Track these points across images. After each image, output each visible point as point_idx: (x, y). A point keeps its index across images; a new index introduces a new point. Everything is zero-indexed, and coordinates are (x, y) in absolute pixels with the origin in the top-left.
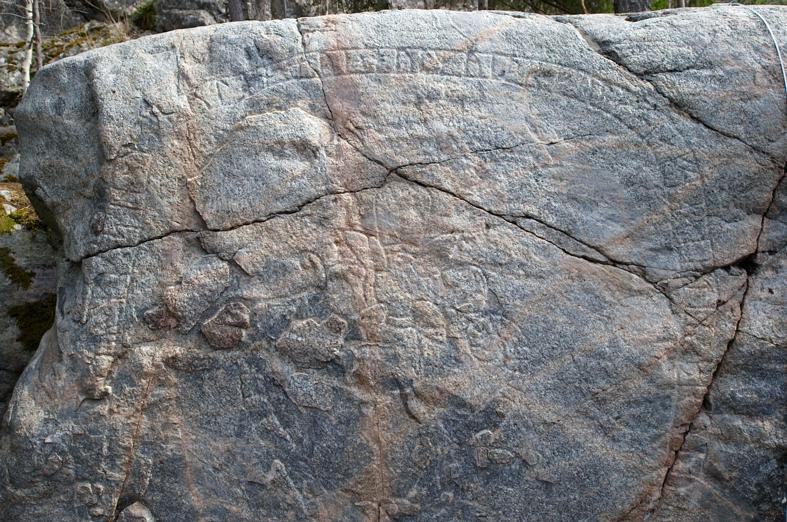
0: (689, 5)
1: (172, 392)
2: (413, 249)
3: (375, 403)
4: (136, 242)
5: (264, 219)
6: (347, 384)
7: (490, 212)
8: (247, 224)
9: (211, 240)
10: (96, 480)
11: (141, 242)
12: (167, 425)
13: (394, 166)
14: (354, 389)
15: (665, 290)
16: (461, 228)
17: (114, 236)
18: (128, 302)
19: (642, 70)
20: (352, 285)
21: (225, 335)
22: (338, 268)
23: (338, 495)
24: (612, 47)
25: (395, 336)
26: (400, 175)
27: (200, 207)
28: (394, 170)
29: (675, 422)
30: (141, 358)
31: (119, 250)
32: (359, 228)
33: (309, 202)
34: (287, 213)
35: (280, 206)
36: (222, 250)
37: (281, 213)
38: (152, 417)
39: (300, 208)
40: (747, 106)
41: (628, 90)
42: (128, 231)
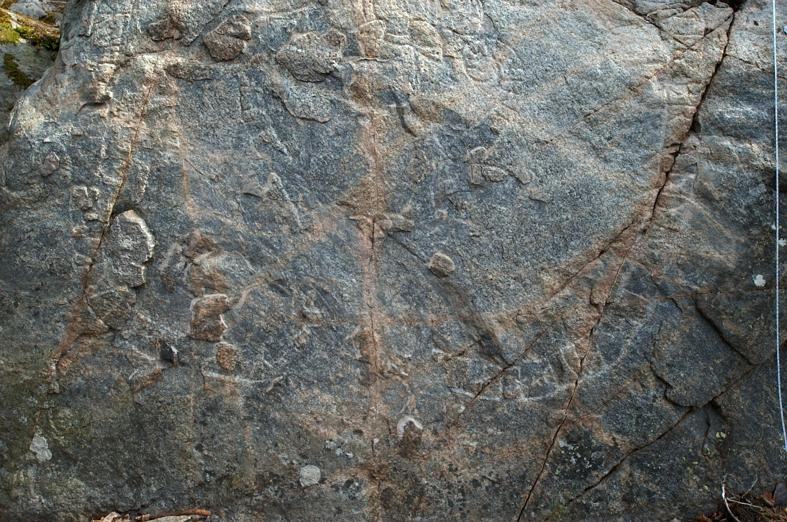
1: (172, 100)
3: (372, 115)
6: (344, 96)
12: (165, 133)
14: (351, 103)
18: (132, 17)
21: (227, 45)
29: (665, 142)
38: (151, 124)
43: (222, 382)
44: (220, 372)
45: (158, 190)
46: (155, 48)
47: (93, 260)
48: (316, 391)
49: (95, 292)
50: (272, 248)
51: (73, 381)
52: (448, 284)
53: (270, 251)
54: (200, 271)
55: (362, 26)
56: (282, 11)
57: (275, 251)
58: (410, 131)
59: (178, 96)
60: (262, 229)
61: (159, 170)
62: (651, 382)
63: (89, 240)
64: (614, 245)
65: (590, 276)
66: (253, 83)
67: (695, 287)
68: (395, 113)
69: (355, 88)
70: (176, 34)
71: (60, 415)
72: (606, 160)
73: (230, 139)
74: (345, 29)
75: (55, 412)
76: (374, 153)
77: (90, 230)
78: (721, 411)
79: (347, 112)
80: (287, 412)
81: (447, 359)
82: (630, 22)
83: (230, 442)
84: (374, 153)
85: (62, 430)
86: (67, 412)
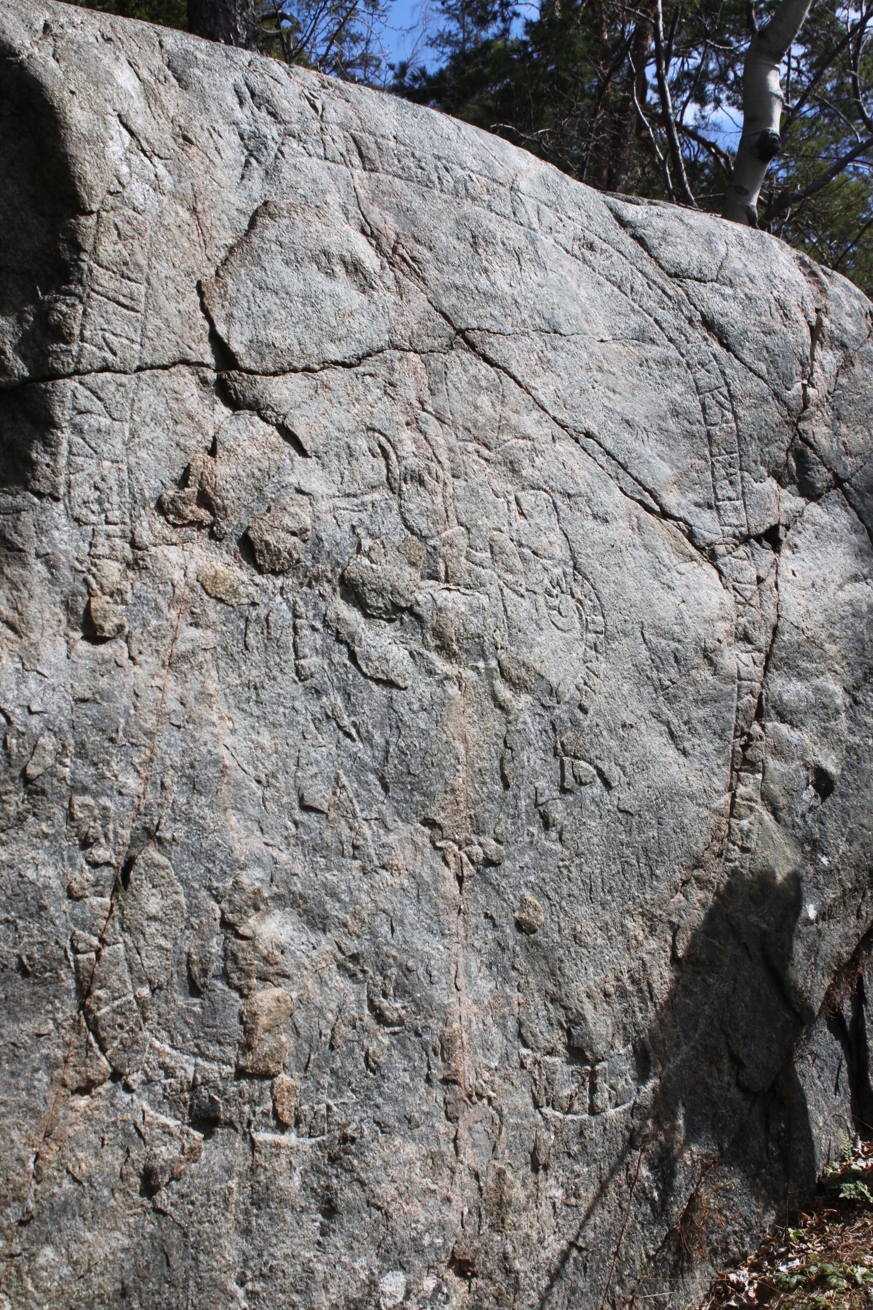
0: (473, 85)
1: (207, 637)
2: (485, 452)
3: (459, 678)
4: (134, 366)
5: (317, 367)
6: (426, 646)
7: (554, 419)
8: (295, 370)
9: (239, 383)
10: (103, 793)
11: (140, 369)
12: (205, 697)
13: (463, 326)
14: (433, 656)
15: (713, 557)
16: (533, 436)
17: (101, 349)
18: (130, 471)
19: (673, 271)
20: (432, 493)
21: (281, 546)
22: (412, 462)
23: (416, 830)
24: (640, 231)
25: (477, 578)
26: (467, 341)
27: (221, 329)
28: (460, 332)
29: (736, 730)
30: (171, 570)
31: (108, 375)
32: (430, 409)
33: (370, 355)
34: (344, 365)
35: (334, 352)
36: (268, 407)
37: (336, 363)
38: (182, 679)
39: (360, 359)
40: (767, 340)
41: (664, 292)
42: (122, 345)
43: (278, 1146)
44: (274, 1130)
45: (188, 803)
46: (175, 538)
47: (102, 940)
48: (398, 1141)
49: (106, 1004)
50: (340, 900)
51: (56, 1189)
52: (536, 944)
53: (337, 905)
54: (255, 948)
55: (443, 535)
56: (348, 495)
57: (344, 906)
58: (501, 708)
59: (215, 631)
60: (328, 869)
61: (192, 767)
62: (726, 1064)
63: (95, 901)
64: (696, 872)
65: (675, 919)
66: (311, 614)
67: (764, 926)
68: (484, 677)
69: (438, 634)
70: (204, 514)
71: (41, 1261)
72: (685, 753)
73: (281, 710)
74: (426, 537)
75: (33, 1256)
76: (465, 740)
77: (96, 884)
78: (673, 1174)
79: (431, 673)
80: (362, 1184)
81: (536, 1062)
82: (692, 559)
83: (286, 1256)
84: (465, 740)
85: (46, 1291)
86: (48, 1252)
